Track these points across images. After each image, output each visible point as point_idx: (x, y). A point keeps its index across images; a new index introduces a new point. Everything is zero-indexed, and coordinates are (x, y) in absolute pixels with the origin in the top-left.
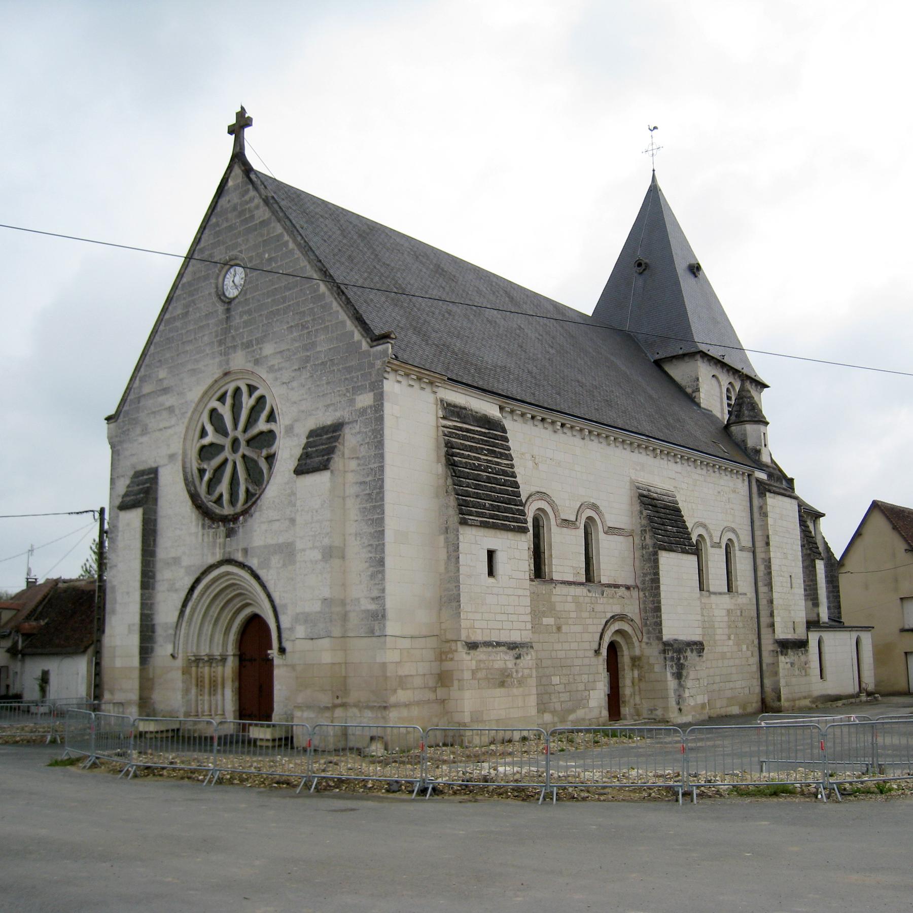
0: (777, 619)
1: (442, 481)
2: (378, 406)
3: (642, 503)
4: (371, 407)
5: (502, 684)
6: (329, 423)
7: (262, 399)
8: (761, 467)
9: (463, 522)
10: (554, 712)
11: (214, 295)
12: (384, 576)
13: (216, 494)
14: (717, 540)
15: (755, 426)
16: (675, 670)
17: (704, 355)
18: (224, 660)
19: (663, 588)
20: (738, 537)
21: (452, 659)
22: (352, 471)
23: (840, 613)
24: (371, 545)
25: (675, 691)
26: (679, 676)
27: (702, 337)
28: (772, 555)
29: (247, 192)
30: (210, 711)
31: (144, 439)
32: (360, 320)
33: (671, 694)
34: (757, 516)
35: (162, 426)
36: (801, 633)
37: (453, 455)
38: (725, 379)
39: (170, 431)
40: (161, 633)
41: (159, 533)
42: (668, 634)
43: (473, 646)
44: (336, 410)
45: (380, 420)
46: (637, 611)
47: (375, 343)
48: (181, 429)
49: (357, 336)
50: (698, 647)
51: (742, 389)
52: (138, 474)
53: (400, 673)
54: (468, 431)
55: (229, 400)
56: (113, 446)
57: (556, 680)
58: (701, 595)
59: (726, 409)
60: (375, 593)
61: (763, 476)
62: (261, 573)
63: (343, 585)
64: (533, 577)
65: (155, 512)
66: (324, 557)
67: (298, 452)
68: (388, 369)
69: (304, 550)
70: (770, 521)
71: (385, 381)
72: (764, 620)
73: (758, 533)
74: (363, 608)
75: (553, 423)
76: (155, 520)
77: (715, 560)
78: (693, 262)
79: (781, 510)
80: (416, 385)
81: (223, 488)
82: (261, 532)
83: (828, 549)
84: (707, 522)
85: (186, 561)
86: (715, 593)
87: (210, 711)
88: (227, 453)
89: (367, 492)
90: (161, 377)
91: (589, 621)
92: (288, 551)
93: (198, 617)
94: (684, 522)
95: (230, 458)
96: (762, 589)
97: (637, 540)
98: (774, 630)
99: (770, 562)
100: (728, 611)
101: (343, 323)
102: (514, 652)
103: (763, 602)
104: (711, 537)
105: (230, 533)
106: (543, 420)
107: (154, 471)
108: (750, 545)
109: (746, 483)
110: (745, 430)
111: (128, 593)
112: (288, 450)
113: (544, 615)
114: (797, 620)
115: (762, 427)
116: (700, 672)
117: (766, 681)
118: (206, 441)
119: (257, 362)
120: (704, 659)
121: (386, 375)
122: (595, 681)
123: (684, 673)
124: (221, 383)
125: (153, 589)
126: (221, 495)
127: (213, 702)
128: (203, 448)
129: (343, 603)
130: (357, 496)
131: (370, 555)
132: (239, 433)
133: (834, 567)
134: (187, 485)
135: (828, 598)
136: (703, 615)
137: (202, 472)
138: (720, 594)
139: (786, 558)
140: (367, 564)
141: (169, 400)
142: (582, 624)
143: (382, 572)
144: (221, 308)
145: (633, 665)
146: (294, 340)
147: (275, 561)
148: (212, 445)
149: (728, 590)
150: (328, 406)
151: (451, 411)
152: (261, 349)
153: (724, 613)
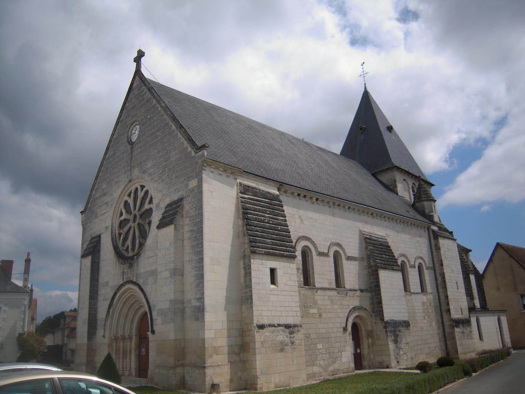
0: (451, 307)
1: (241, 229)
2: (200, 187)
3: (366, 242)
4: (196, 187)
5: (282, 350)
6: (176, 199)
7: (147, 192)
8: (434, 224)
9: (253, 252)
10: (320, 366)
11: (126, 141)
12: (203, 285)
13: (126, 246)
14: (412, 263)
15: (429, 203)
16: (393, 338)
17: (399, 169)
18: (131, 338)
19: (382, 290)
20: (424, 261)
21: (249, 336)
22: (187, 224)
23: (486, 303)
24: (197, 267)
25: (394, 350)
26: (396, 341)
27: (396, 160)
28: (445, 271)
29: (141, 87)
30: (123, 368)
31: (96, 220)
32: (190, 140)
33: (392, 352)
34: (435, 250)
35: (103, 212)
36: (466, 314)
37: (247, 213)
38: (410, 182)
39: (107, 215)
40: (100, 323)
41: (100, 269)
42: (388, 315)
43: (261, 327)
44: (179, 191)
45: (201, 193)
46: (368, 304)
47: (198, 151)
48: (111, 213)
49: (189, 149)
50: (406, 324)
51: (420, 185)
52: (93, 238)
53: (215, 345)
54: (257, 200)
55: (132, 195)
56: (83, 225)
57: (320, 346)
58: (406, 294)
59: (412, 197)
60: (199, 296)
61: (435, 228)
62: (144, 287)
63: (183, 291)
64: (302, 285)
65: (99, 258)
66: (171, 275)
67: (160, 217)
68: (205, 165)
69: (161, 272)
70: (442, 252)
71: (203, 171)
72: (444, 308)
73: (435, 259)
74: (193, 305)
75: (311, 198)
76: (99, 262)
77: (413, 276)
78: (388, 125)
79: (448, 250)
80: (224, 175)
81: (129, 242)
82: (144, 264)
83: (475, 269)
84: (404, 253)
85: (111, 284)
86: (414, 293)
87: (123, 368)
88: (131, 224)
89: (195, 235)
90: (103, 187)
91: (339, 311)
92: (154, 273)
93: (116, 315)
94: (393, 253)
95: (132, 226)
96: (441, 290)
97: (365, 264)
98: (450, 313)
99: (444, 275)
100: (423, 303)
101: (183, 143)
102: (289, 330)
103: (442, 297)
104: (409, 261)
105: (131, 266)
106: (305, 196)
107: (99, 236)
108: (432, 266)
109: (427, 232)
110: (423, 205)
111: (84, 302)
112: (156, 218)
113: (311, 307)
114: (463, 307)
115: (433, 203)
116: (408, 337)
117: (448, 343)
118: (122, 218)
119: (144, 172)
120: (410, 331)
121: (204, 168)
122: (344, 346)
123: (399, 340)
124: (129, 186)
125: (97, 300)
126: (128, 246)
127: (125, 363)
128: (121, 221)
129: (182, 302)
130: (190, 239)
131: (196, 273)
132: (136, 212)
133: (480, 278)
134: (113, 242)
135: (478, 295)
136: (408, 306)
137: (120, 234)
138: (417, 293)
139: (453, 272)
140: (195, 278)
141: (107, 199)
142: (336, 312)
143: (203, 283)
144: (129, 147)
145: (368, 336)
146: (160, 157)
147: (150, 280)
148: (125, 219)
149: (422, 291)
150: (175, 190)
151: (245, 189)
152: (146, 165)
153: (420, 304)
